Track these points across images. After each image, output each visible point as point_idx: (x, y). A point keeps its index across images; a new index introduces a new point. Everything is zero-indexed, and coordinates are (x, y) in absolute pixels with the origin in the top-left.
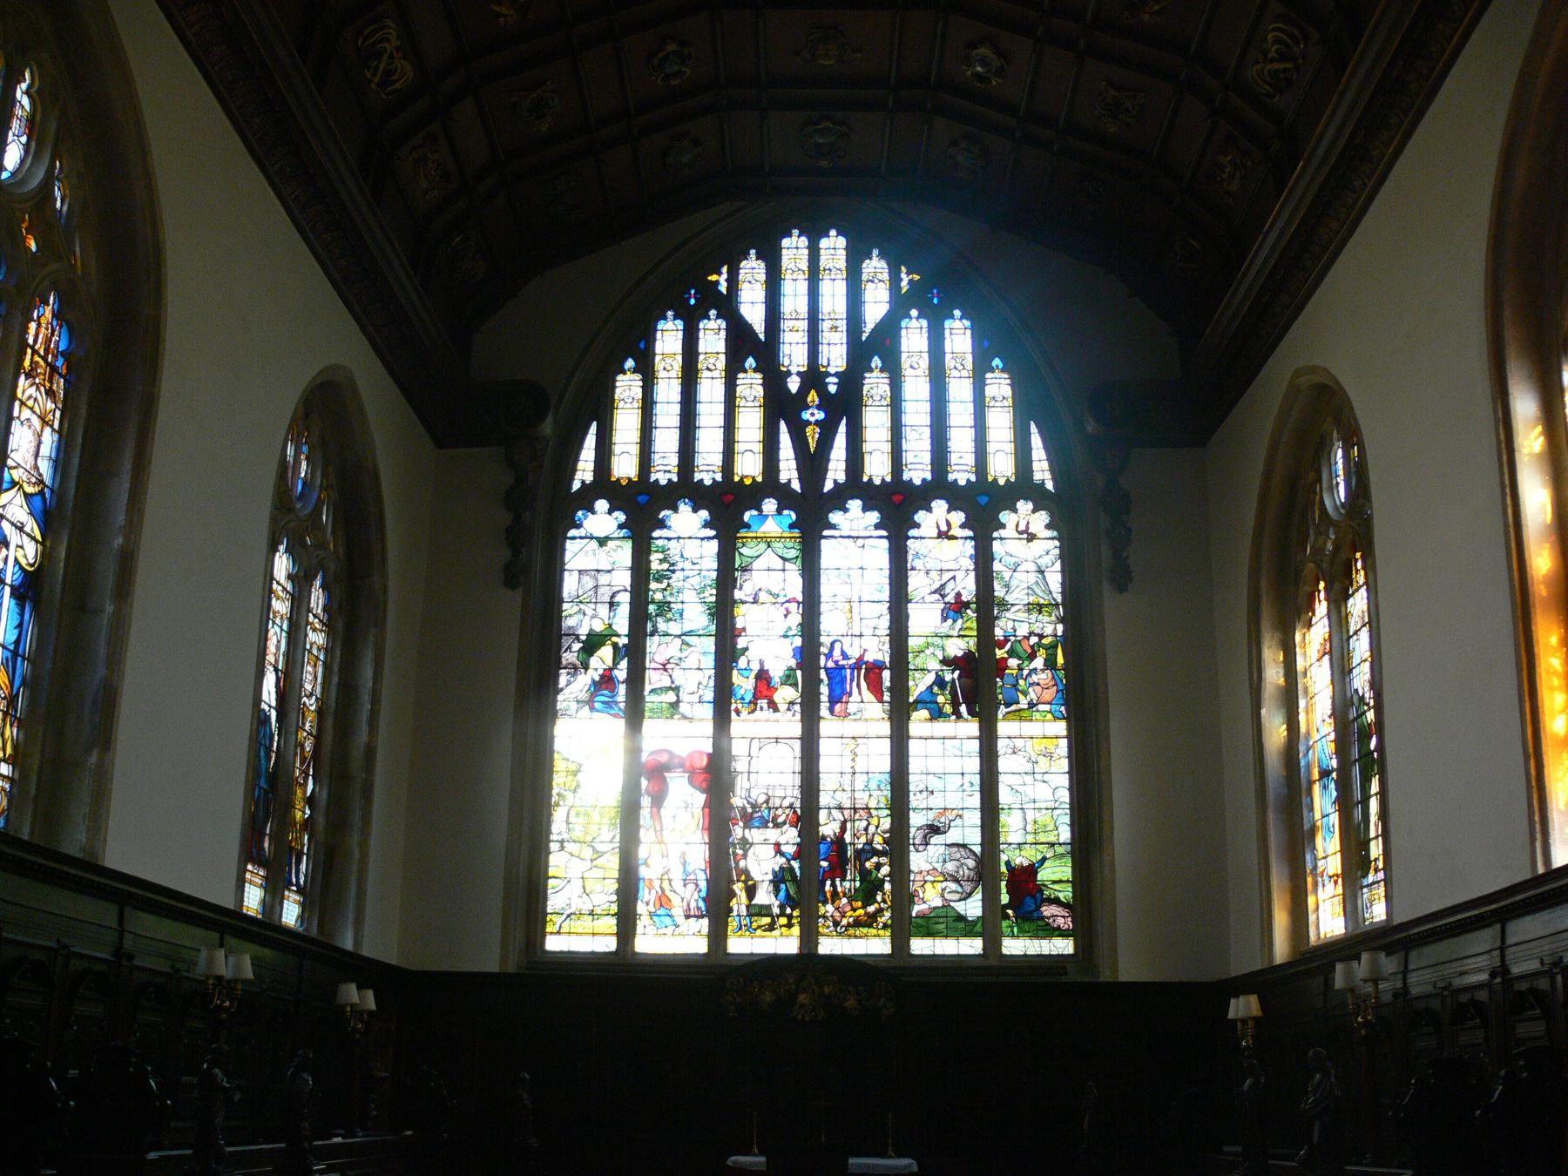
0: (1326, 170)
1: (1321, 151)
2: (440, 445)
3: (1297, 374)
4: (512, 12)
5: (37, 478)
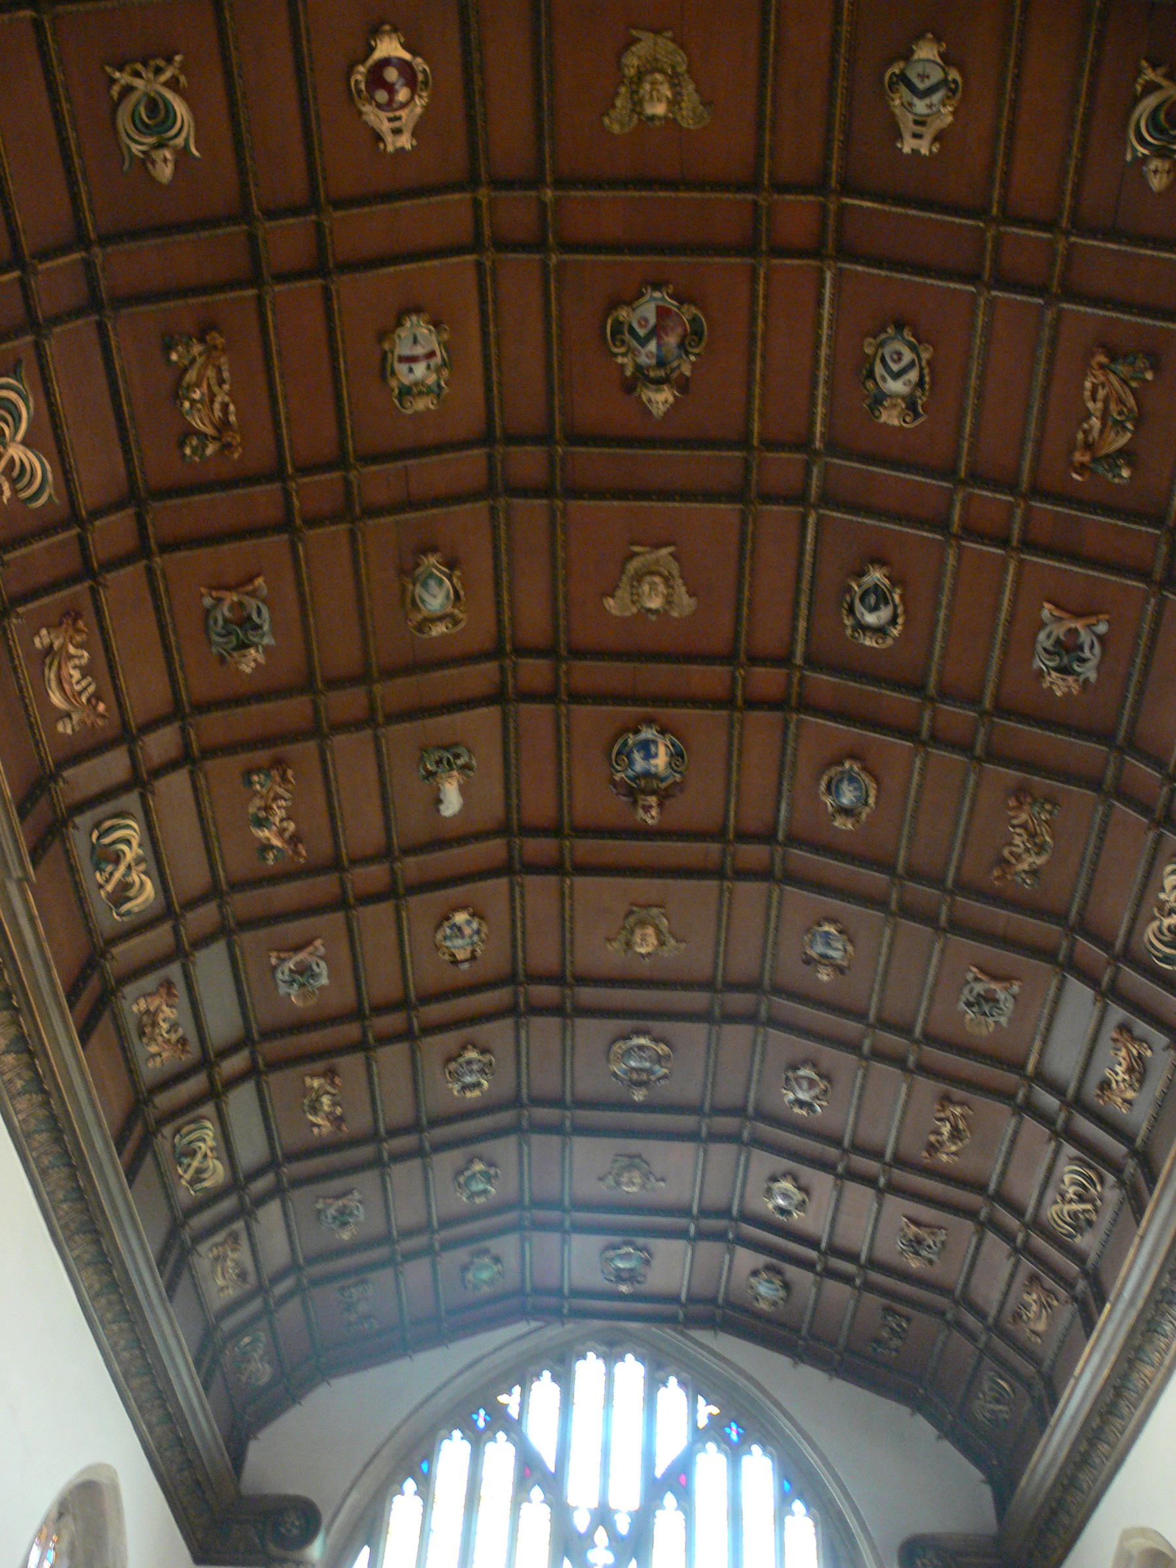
0: (1133, 1314)
1: (1127, 1294)
2: (197, 1560)
3: (1127, 1535)
4: (327, 1123)
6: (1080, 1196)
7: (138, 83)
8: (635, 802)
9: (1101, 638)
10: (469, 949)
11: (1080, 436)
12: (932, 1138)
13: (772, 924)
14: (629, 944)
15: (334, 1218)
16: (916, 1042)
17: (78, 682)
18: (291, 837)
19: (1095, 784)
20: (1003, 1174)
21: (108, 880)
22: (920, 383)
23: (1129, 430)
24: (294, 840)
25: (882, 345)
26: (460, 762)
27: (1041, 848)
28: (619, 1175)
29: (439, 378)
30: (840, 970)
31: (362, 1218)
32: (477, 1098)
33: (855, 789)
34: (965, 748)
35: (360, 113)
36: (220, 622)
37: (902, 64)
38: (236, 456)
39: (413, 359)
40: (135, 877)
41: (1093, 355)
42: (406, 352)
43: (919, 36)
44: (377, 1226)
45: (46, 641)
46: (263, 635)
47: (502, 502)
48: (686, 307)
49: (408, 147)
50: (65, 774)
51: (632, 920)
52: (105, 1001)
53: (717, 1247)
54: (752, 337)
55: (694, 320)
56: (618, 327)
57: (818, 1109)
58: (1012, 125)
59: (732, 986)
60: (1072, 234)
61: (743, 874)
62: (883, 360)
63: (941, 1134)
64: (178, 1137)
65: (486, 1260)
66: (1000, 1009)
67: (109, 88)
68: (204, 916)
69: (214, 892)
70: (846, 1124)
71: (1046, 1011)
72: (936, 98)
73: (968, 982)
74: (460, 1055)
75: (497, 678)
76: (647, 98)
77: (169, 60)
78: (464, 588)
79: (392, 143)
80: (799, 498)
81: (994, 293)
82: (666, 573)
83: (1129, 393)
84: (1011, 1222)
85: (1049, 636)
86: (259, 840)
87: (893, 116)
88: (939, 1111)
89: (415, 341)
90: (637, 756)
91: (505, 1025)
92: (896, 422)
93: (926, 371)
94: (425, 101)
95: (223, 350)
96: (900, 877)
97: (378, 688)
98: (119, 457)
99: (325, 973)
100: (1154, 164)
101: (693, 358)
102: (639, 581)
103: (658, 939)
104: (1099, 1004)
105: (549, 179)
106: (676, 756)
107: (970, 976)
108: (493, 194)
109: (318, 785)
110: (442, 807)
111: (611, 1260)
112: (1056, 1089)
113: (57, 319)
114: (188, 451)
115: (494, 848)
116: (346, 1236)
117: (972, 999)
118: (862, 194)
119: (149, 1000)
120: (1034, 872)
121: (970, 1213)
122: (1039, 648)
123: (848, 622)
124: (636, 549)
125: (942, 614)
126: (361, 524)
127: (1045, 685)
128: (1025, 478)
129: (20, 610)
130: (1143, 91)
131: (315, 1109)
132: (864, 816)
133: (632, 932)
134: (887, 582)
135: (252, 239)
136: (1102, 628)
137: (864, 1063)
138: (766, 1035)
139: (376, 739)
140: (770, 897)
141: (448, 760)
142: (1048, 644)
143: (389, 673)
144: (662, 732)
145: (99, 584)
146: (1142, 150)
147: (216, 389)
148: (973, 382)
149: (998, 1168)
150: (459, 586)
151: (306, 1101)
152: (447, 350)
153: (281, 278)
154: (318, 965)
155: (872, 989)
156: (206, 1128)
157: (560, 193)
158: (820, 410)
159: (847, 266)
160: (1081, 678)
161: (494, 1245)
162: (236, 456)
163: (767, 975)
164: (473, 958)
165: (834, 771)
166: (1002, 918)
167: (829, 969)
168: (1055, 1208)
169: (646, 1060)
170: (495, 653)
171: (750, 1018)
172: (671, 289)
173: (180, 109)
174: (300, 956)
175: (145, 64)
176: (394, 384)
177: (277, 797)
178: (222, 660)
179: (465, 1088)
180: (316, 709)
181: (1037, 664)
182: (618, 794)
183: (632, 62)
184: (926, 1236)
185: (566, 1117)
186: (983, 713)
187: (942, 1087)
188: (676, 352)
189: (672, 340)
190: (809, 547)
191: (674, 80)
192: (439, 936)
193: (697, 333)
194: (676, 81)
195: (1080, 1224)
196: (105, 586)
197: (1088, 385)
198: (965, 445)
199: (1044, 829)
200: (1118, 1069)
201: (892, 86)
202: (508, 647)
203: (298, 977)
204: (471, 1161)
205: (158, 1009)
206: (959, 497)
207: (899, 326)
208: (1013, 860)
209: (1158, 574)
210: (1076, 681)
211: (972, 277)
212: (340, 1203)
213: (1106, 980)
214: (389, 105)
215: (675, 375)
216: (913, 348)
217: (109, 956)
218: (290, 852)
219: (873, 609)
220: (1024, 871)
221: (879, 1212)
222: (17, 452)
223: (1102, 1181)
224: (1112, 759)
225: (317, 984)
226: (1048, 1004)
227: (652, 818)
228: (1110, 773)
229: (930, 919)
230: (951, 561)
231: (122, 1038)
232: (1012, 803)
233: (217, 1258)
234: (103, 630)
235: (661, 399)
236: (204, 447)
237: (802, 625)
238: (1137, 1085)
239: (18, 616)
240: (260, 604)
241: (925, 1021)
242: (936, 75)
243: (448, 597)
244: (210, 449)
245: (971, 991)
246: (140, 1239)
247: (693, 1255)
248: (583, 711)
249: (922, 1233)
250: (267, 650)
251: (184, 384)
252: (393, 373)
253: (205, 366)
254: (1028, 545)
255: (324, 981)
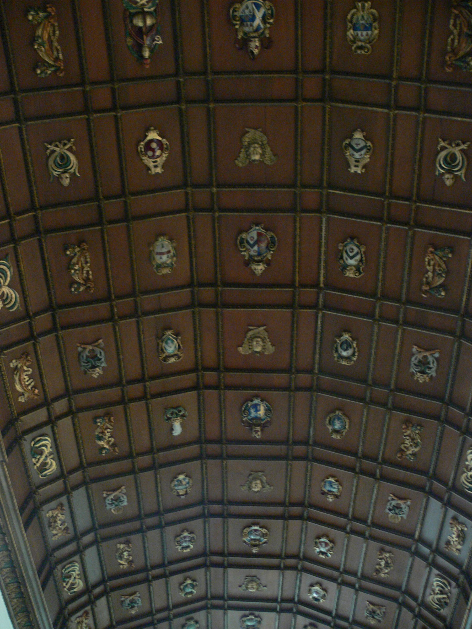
4: (126, 563)
5: (80, 257)
6: (441, 591)
7: (57, 149)
8: (251, 429)
9: (436, 359)
10: (185, 490)
11: (425, 279)
12: (377, 567)
13: (308, 478)
14: (250, 488)
15: (129, 604)
16: (368, 526)
17: (27, 381)
18: (113, 444)
19: (436, 417)
20: (408, 582)
21: (37, 462)
22: (361, 261)
23: (444, 277)
24: (114, 445)
25: (345, 246)
26: (181, 413)
27: (416, 445)
28: (247, 585)
29: (172, 261)
30: (336, 496)
31: (140, 604)
32: (189, 552)
33: (341, 422)
34: (384, 405)
35: (142, 160)
36: (85, 357)
37: (349, 140)
38: (92, 291)
39: (162, 254)
40: (49, 461)
41: (428, 248)
42: (159, 251)
43: (355, 130)
44: (147, 608)
45: (15, 364)
46: (101, 363)
47: (197, 309)
48: (268, 233)
49: (160, 172)
50: (22, 418)
51: (251, 477)
52: (36, 511)
53: (289, 615)
54: (295, 245)
55: (272, 238)
56: (242, 241)
57: (329, 555)
58: (392, 162)
59: (292, 504)
60: (417, 202)
61: (296, 458)
62: (346, 252)
63: (381, 565)
64: (64, 570)
65: (192, 622)
66: (403, 511)
67: (46, 151)
68: (76, 477)
69: (81, 467)
70: (341, 562)
71: (422, 512)
72: (363, 152)
73: (389, 501)
74: (182, 534)
75: (195, 379)
76: (252, 153)
77: (69, 141)
78: (182, 344)
79: (154, 171)
80: (315, 306)
81: (388, 225)
82: (262, 337)
83: (443, 263)
84: (413, 603)
85: (416, 359)
86: (99, 445)
87: (347, 158)
88: (380, 555)
89: (163, 247)
90: (252, 411)
91: (199, 522)
92: (352, 276)
93: (363, 256)
94: (166, 155)
95: (87, 250)
96: (360, 458)
97: (148, 384)
98: (46, 293)
99: (126, 500)
100: (447, 176)
101: (272, 252)
102: (252, 340)
103: (262, 485)
104: (444, 509)
105: (215, 184)
106: (268, 410)
107: (390, 498)
108: (193, 190)
109: (123, 421)
110: (173, 432)
111: (245, 621)
112: (428, 545)
113: (24, 238)
114: (73, 290)
115: (194, 449)
116: (133, 612)
117: (391, 508)
118: (336, 189)
119: (54, 511)
120: (414, 454)
121: (395, 599)
122: (412, 363)
123: (336, 355)
124: (251, 328)
125: (373, 351)
126: (141, 319)
127: (415, 379)
128: (404, 296)
129: (5, 352)
130: (441, 149)
131: (121, 557)
132: (344, 433)
133: (251, 483)
134: (350, 339)
135: (99, 207)
136: (437, 355)
137: (348, 535)
138: (307, 524)
139: (147, 405)
140: (307, 467)
141: (176, 413)
142: (416, 362)
143: (152, 378)
144: (262, 401)
145: (37, 342)
146: (442, 171)
147: (84, 265)
148: (382, 259)
149: (406, 579)
150: (180, 343)
151: (117, 554)
152: (175, 250)
153: (110, 222)
154: (123, 497)
155: (350, 504)
156: (76, 566)
157: (218, 189)
158: (322, 272)
159: (331, 216)
160: (430, 375)
161: (196, 615)
162: (92, 291)
163: (307, 499)
164: (186, 494)
165: (331, 415)
166: (402, 474)
167: (332, 497)
168: (431, 597)
169: (258, 536)
170: (195, 370)
171: (300, 517)
172: (263, 225)
173: (73, 158)
174: (115, 493)
175: (60, 142)
176: (154, 263)
177: (107, 428)
178: (85, 373)
179: (183, 548)
180: (123, 391)
181: (412, 370)
182: (245, 426)
183: (246, 140)
184: (377, 610)
185: (226, 560)
186: (391, 390)
187: (380, 545)
188: (265, 250)
189: (263, 245)
190: (319, 326)
191: (262, 146)
192: (173, 485)
193: (273, 243)
194: (263, 147)
195: (442, 604)
196: (39, 343)
197: (427, 260)
198: (380, 284)
199: (417, 437)
200: (454, 536)
201: (345, 147)
202: (200, 367)
203: (114, 502)
204: (186, 579)
205: (57, 516)
206: (378, 305)
207: (352, 239)
208: (405, 450)
209: (458, 333)
210: (427, 376)
211: (380, 219)
212: (131, 598)
213: (446, 498)
214: (153, 157)
215: (265, 259)
216: (358, 247)
217: (37, 493)
218: (112, 451)
219: (346, 350)
220: (410, 454)
221: (356, 599)
222: (6, 290)
223: (450, 585)
224: (443, 407)
225: (123, 505)
226: (423, 509)
227: (258, 435)
228: (443, 413)
229: (372, 475)
230: (376, 330)
231: (42, 528)
232: (404, 426)
233: (79, 623)
234: (38, 360)
235: (259, 268)
236: (79, 288)
237: (317, 356)
238: (462, 543)
239: (4, 355)
240: (101, 350)
241: (372, 517)
242: (362, 144)
243: (175, 347)
244: (82, 289)
245: (391, 504)
246: (46, 615)
247: (279, 620)
248: (230, 393)
249: (375, 608)
250: (103, 368)
251: (72, 263)
252: (154, 259)
253: (80, 257)
254: (406, 323)
255: (125, 503)
